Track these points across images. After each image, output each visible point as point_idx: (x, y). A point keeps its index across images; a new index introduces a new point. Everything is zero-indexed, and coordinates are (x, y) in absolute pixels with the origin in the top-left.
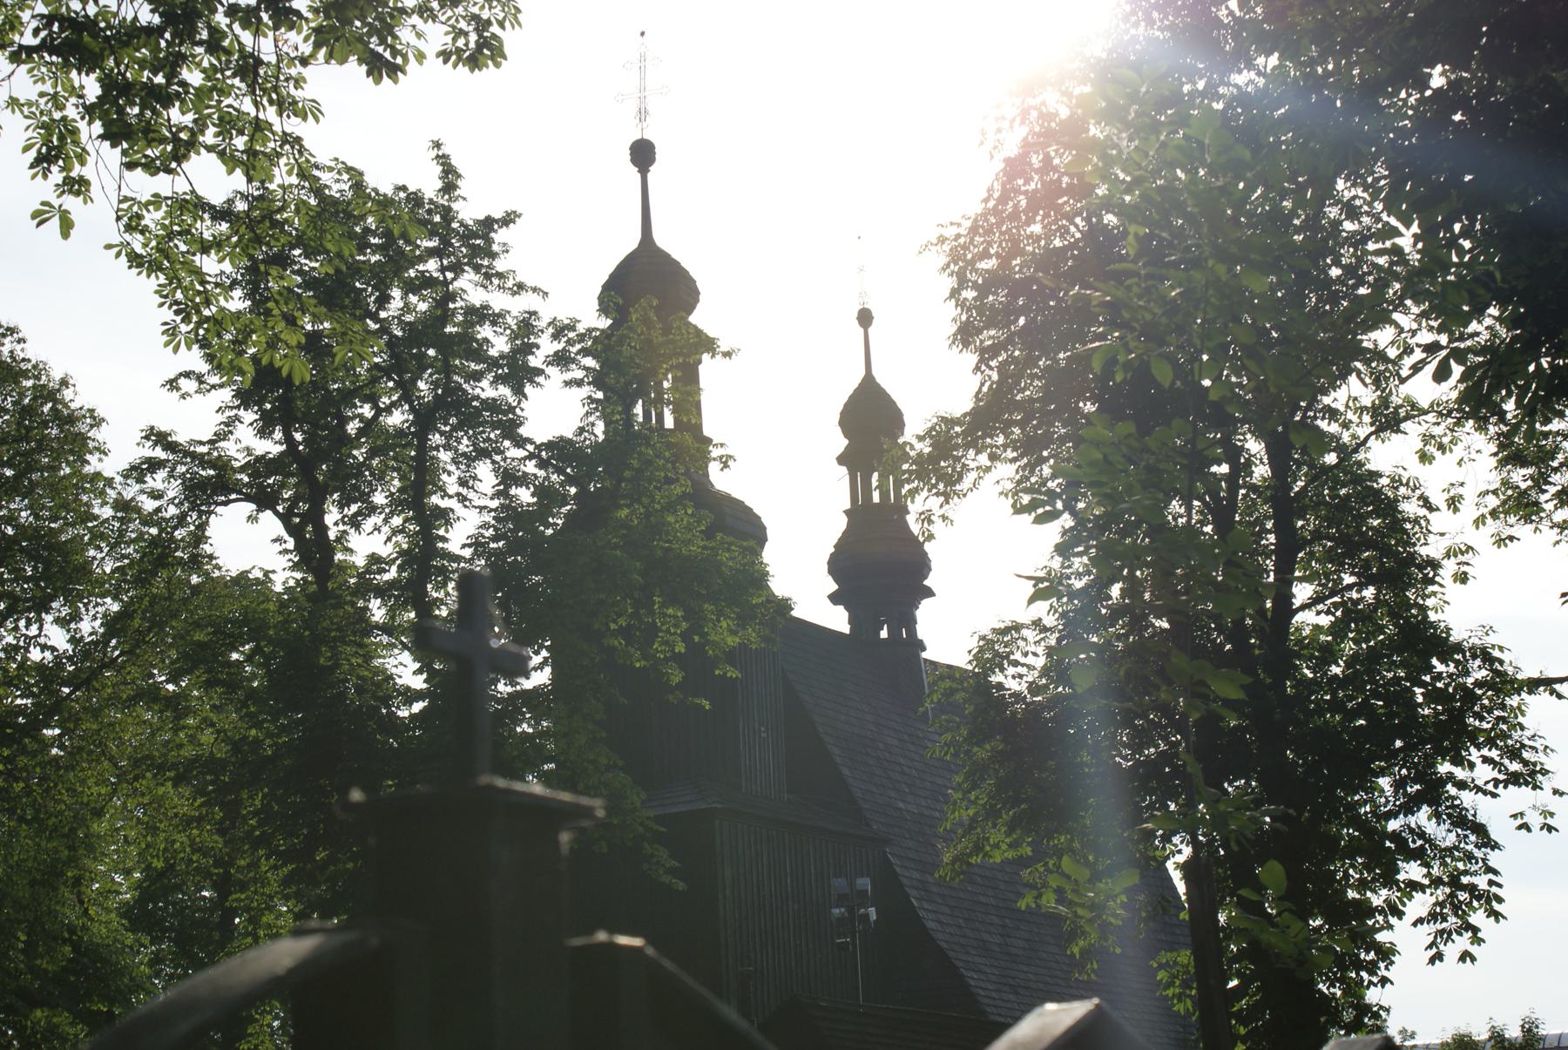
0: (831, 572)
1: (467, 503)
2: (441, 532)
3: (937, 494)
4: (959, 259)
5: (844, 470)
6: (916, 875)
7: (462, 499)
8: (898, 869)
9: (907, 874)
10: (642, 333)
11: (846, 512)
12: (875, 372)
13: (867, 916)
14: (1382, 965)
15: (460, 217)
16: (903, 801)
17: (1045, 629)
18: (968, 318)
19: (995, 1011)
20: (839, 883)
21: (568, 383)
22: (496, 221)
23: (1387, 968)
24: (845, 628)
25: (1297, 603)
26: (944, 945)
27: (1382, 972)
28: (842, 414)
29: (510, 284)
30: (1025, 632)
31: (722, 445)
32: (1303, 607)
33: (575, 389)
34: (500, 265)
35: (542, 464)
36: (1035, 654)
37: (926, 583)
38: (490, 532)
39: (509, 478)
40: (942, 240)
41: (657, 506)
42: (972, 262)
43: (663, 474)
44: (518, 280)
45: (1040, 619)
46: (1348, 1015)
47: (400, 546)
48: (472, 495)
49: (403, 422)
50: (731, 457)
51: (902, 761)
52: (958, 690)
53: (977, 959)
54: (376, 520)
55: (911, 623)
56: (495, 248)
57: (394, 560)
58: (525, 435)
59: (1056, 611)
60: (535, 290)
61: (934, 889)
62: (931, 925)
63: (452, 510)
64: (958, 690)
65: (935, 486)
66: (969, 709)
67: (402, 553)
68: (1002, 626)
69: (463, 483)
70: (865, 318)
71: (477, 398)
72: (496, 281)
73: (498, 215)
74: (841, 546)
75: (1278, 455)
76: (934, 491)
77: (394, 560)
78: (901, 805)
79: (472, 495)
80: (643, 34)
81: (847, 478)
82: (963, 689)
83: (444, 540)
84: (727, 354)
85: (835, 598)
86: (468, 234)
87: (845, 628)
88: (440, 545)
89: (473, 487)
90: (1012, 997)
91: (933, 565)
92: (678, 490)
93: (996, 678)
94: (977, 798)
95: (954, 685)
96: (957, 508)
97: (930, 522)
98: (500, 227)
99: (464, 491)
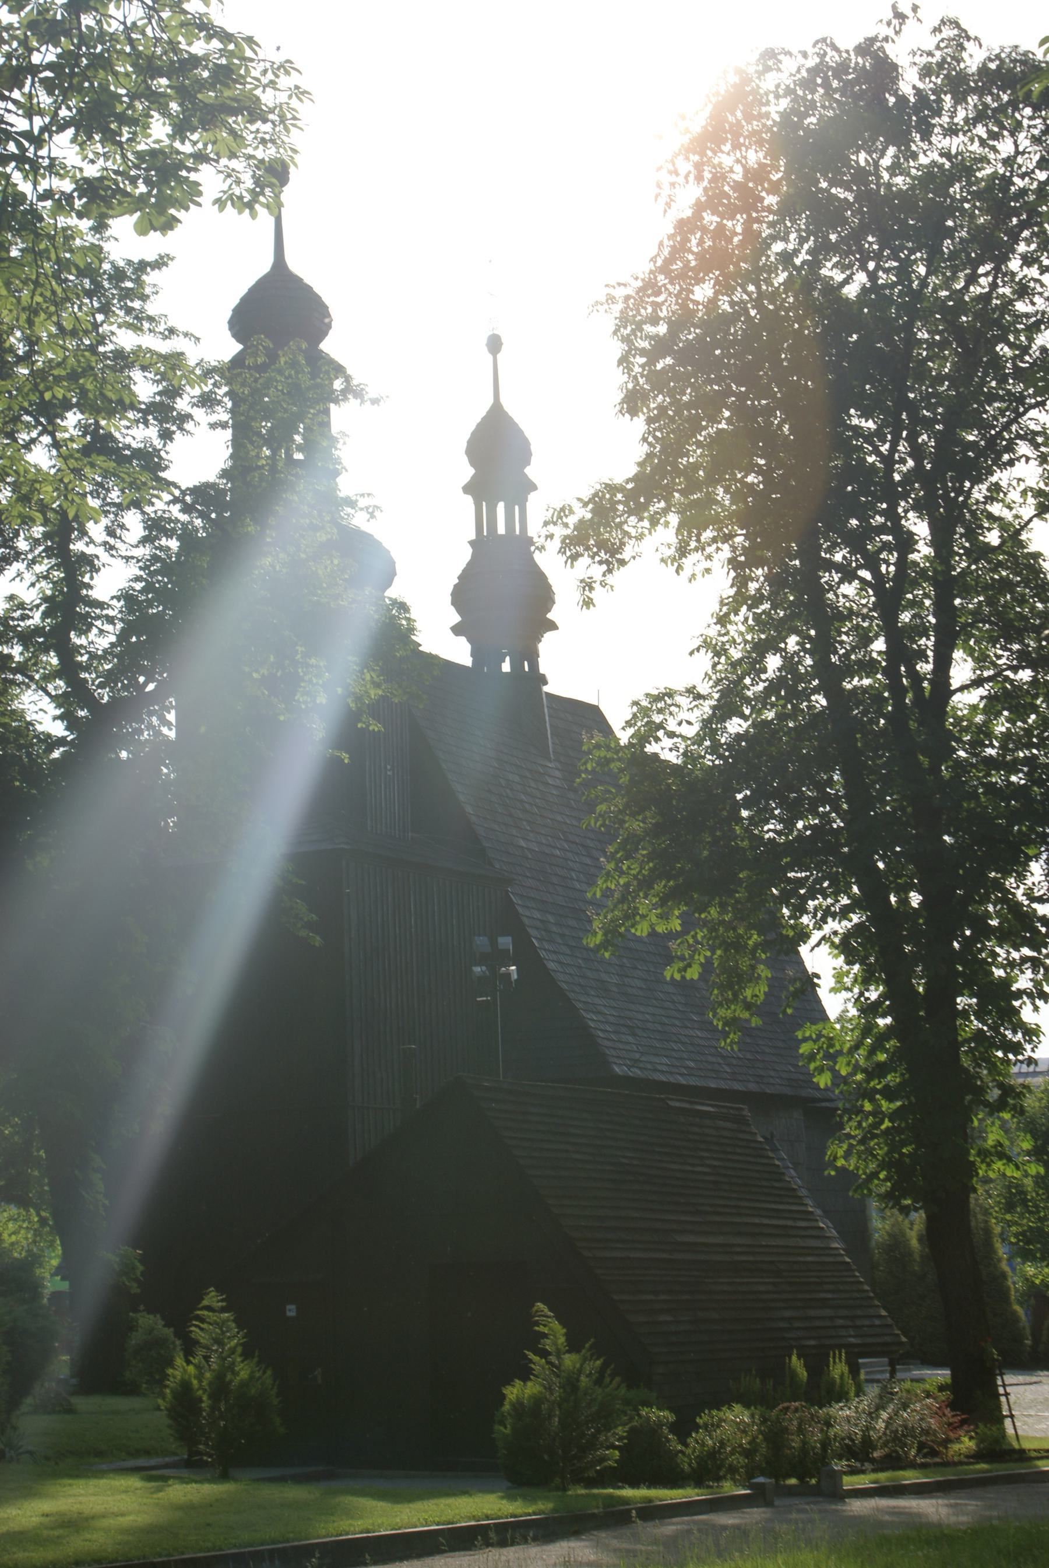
0: (454, 603)
1: (114, 552)
2: (86, 579)
3: (601, 563)
4: (627, 321)
5: (469, 500)
6: (537, 915)
7: (109, 548)
8: (520, 910)
9: (528, 913)
10: (290, 376)
11: (471, 543)
12: (503, 400)
13: (508, 975)
14: (1028, 1047)
15: (111, 258)
16: (524, 839)
17: (699, 697)
18: (634, 387)
19: (614, 1053)
20: (481, 942)
21: (213, 426)
22: (148, 264)
23: (1033, 1051)
24: (467, 661)
25: (955, 684)
26: (564, 986)
27: (1028, 1053)
28: (469, 442)
29: (161, 328)
30: (679, 699)
31: (369, 495)
32: (962, 688)
33: (219, 430)
34: (152, 308)
35: (187, 509)
36: (689, 723)
37: (549, 616)
38: (138, 586)
39: (156, 527)
40: (611, 299)
41: (303, 556)
42: (639, 327)
43: (308, 521)
44: (170, 324)
45: (694, 687)
46: (994, 1094)
47: (43, 592)
48: (119, 544)
49: (50, 467)
50: (378, 508)
51: (523, 797)
52: (613, 760)
53: (597, 1001)
54: (17, 566)
55: (533, 657)
56: (148, 290)
57: (38, 606)
58: (170, 479)
59: (710, 679)
60: (186, 335)
61: (554, 929)
62: (551, 965)
63: (97, 557)
64: (613, 760)
65: (596, 554)
66: (624, 780)
67: (45, 599)
68: (656, 692)
69: (110, 532)
70: (495, 345)
71: (128, 447)
72: (146, 325)
73: (151, 258)
74: (467, 578)
75: (941, 539)
76: (597, 558)
77: (38, 606)
78: (522, 843)
79: (119, 544)
80: (278, 48)
81: (473, 507)
82: (620, 759)
83: (89, 587)
84: (375, 401)
85: (457, 630)
86: (118, 275)
87: (467, 661)
88: (84, 592)
89: (120, 538)
90: (631, 1039)
91: (557, 598)
92: (322, 537)
93: (651, 748)
94: (629, 868)
95: (609, 755)
96: (619, 576)
97: (591, 589)
98: (153, 269)
99: (112, 541)
